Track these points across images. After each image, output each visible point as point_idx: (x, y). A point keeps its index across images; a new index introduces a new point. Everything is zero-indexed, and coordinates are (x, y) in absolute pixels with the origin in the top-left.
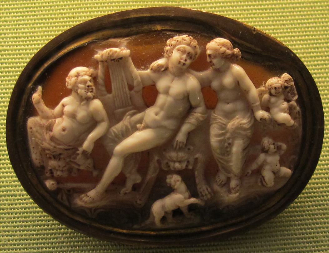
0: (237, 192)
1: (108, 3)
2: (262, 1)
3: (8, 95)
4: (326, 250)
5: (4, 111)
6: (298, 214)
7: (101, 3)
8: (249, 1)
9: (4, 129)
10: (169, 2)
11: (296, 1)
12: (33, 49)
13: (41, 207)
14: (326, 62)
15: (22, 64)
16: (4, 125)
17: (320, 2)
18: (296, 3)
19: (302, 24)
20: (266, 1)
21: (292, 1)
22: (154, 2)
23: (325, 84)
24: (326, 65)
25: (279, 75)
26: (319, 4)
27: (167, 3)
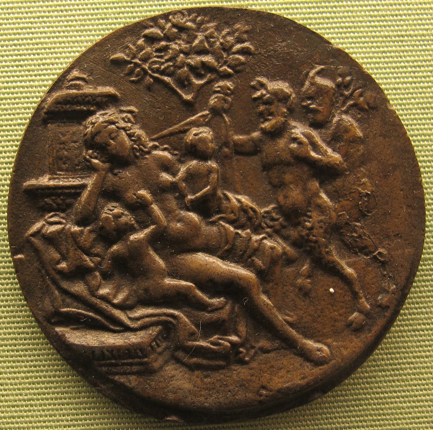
0: (348, 166)
1: (104, 4)
2: (355, 2)
3: (28, 116)
4: (432, 428)
5: (4, 212)
6: (379, 369)
7: (92, 4)
8: (32, 2)
9: (14, 158)
10: (213, 2)
11: (273, 1)
12: (68, 58)
13: (347, 54)
14: (430, 100)
15: (52, 77)
16: (15, 274)
17: (316, 3)
18: (273, 4)
19: (409, 15)
20: (140, 2)
21: (268, 1)
22: (222, 2)
23: (429, 115)
24: (430, 103)
25: (219, 298)
26: (102, 6)
27: (238, 3)
